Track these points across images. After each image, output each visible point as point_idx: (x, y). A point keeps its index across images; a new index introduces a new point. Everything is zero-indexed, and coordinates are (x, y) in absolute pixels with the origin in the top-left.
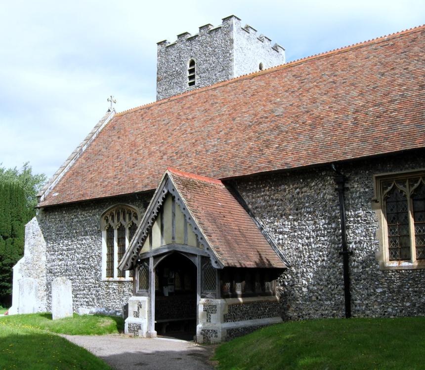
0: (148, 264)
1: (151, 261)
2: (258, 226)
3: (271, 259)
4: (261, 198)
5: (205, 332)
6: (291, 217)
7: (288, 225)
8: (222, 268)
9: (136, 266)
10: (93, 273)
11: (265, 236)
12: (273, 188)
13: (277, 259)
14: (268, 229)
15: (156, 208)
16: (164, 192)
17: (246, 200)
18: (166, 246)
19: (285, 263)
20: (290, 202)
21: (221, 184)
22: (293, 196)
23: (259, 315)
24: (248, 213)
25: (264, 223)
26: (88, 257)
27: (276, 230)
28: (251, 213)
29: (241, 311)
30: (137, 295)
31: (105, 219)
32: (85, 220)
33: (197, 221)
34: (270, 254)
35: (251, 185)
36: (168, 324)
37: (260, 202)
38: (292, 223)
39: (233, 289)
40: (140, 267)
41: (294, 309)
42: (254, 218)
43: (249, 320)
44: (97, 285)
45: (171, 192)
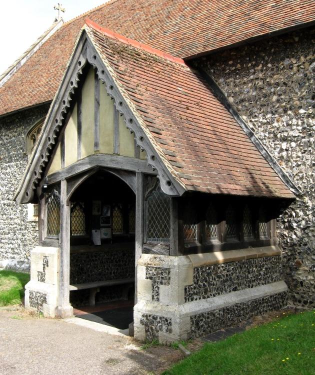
0: (60, 193)
1: (64, 185)
2: (245, 130)
3: (270, 182)
4: (250, 85)
5: (150, 320)
6: (302, 111)
7: (297, 125)
8: (181, 194)
9: (42, 196)
10: (18, 211)
11: (257, 145)
12: (270, 65)
13: (278, 183)
14: (262, 134)
15: (67, 94)
16: (80, 63)
17: (225, 90)
18: (87, 160)
19: (293, 190)
20: (301, 86)
21: (184, 64)
22: (306, 75)
23: (250, 282)
24: (229, 111)
25: (254, 125)
26: (13, 189)
27: (275, 136)
28: (233, 110)
29: (219, 277)
30: (44, 244)
31: (32, 139)
32: (9, 142)
33: (132, 106)
34: (267, 174)
35: (232, 65)
36: (98, 291)
37: (249, 91)
38: (305, 120)
39: (204, 237)
40: (48, 198)
41: (306, 268)
42: (238, 117)
43: (233, 293)
44: (23, 227)
45: (91, 61)
